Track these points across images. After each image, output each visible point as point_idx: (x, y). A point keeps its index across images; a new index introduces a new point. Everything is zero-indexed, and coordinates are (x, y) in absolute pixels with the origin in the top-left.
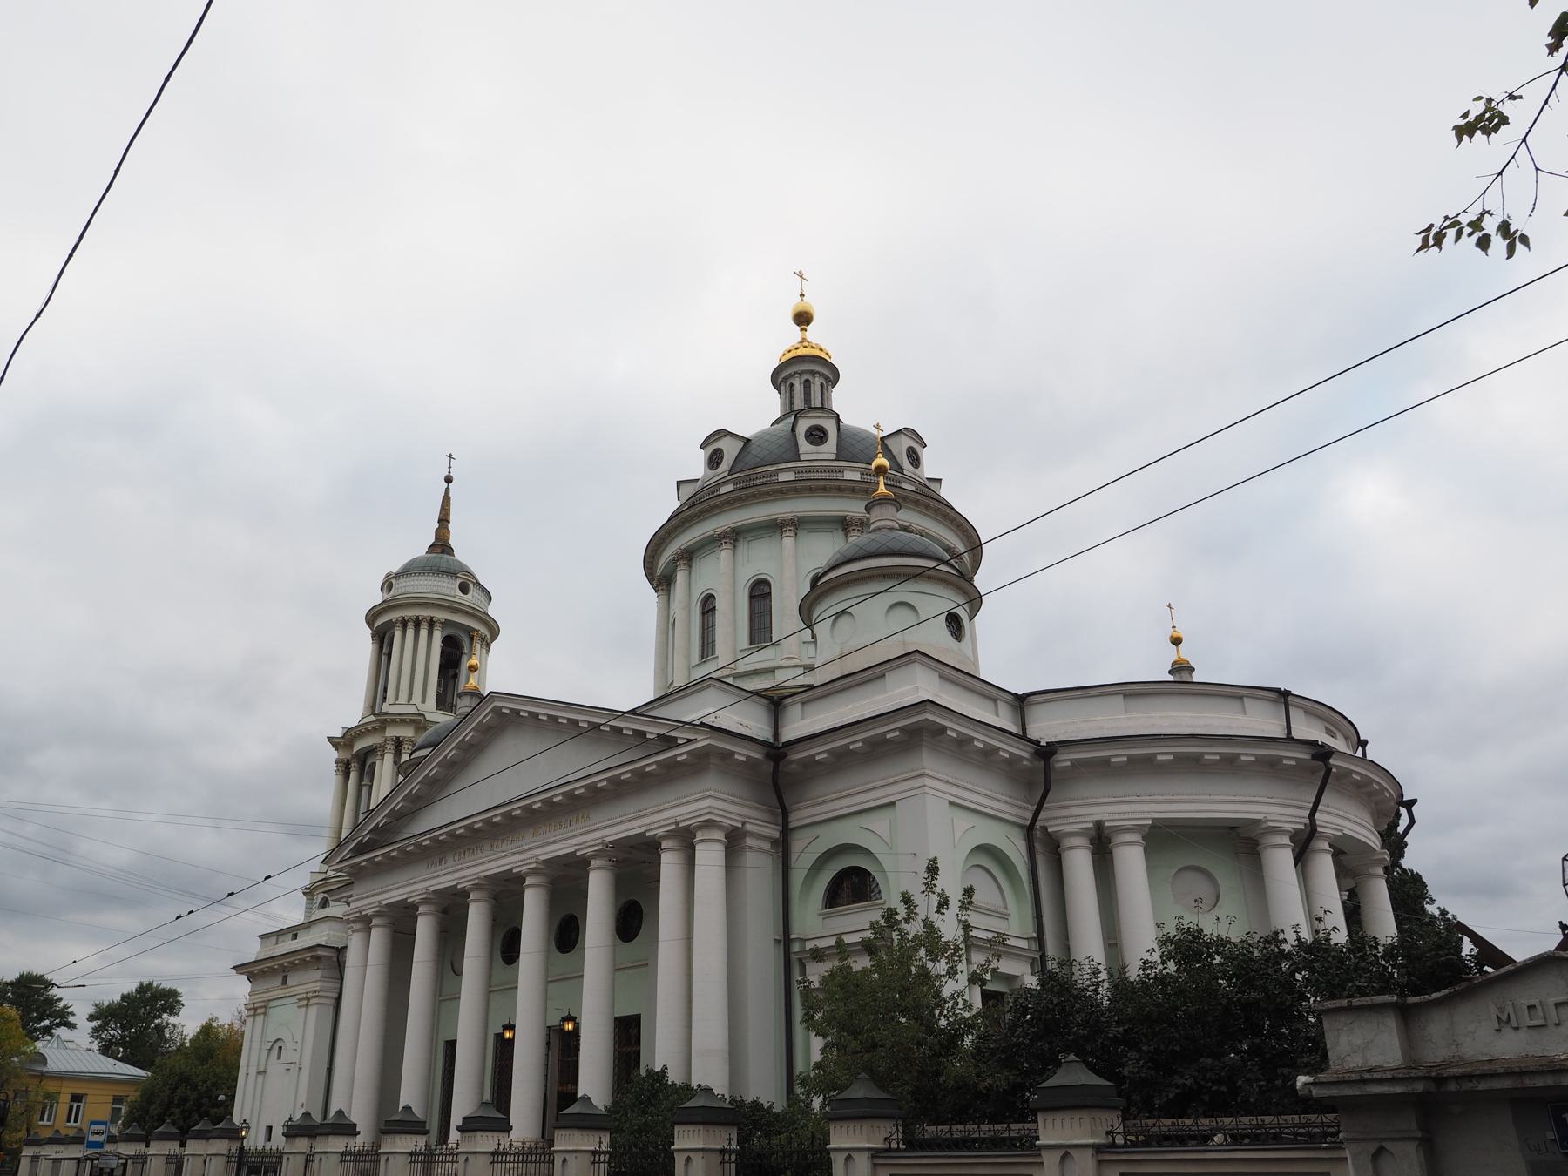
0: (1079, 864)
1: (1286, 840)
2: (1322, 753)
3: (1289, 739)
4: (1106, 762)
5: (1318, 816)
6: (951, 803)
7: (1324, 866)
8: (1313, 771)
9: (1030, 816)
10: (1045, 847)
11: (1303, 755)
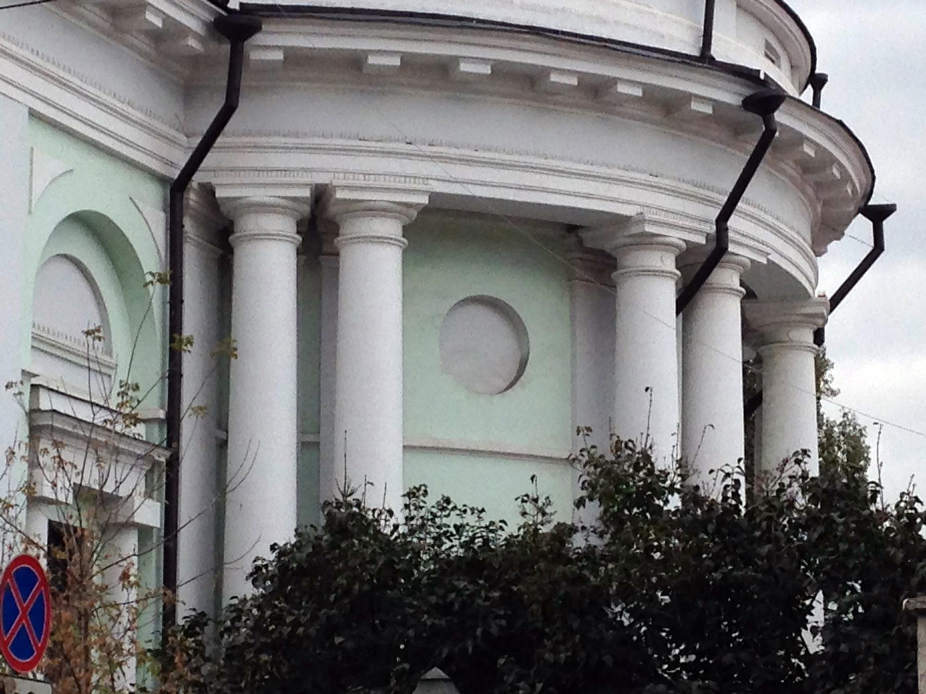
0: (270, 268)
1: (669, 263)
2: (763, 99)
3: (704, 60)
4: (354, 63)
5: (733, 222)
6: (33, 114)
7: (724, 316)
8: (737, 130)
9: (182, 159)
10: (205, 226)
11: (729, 95)
